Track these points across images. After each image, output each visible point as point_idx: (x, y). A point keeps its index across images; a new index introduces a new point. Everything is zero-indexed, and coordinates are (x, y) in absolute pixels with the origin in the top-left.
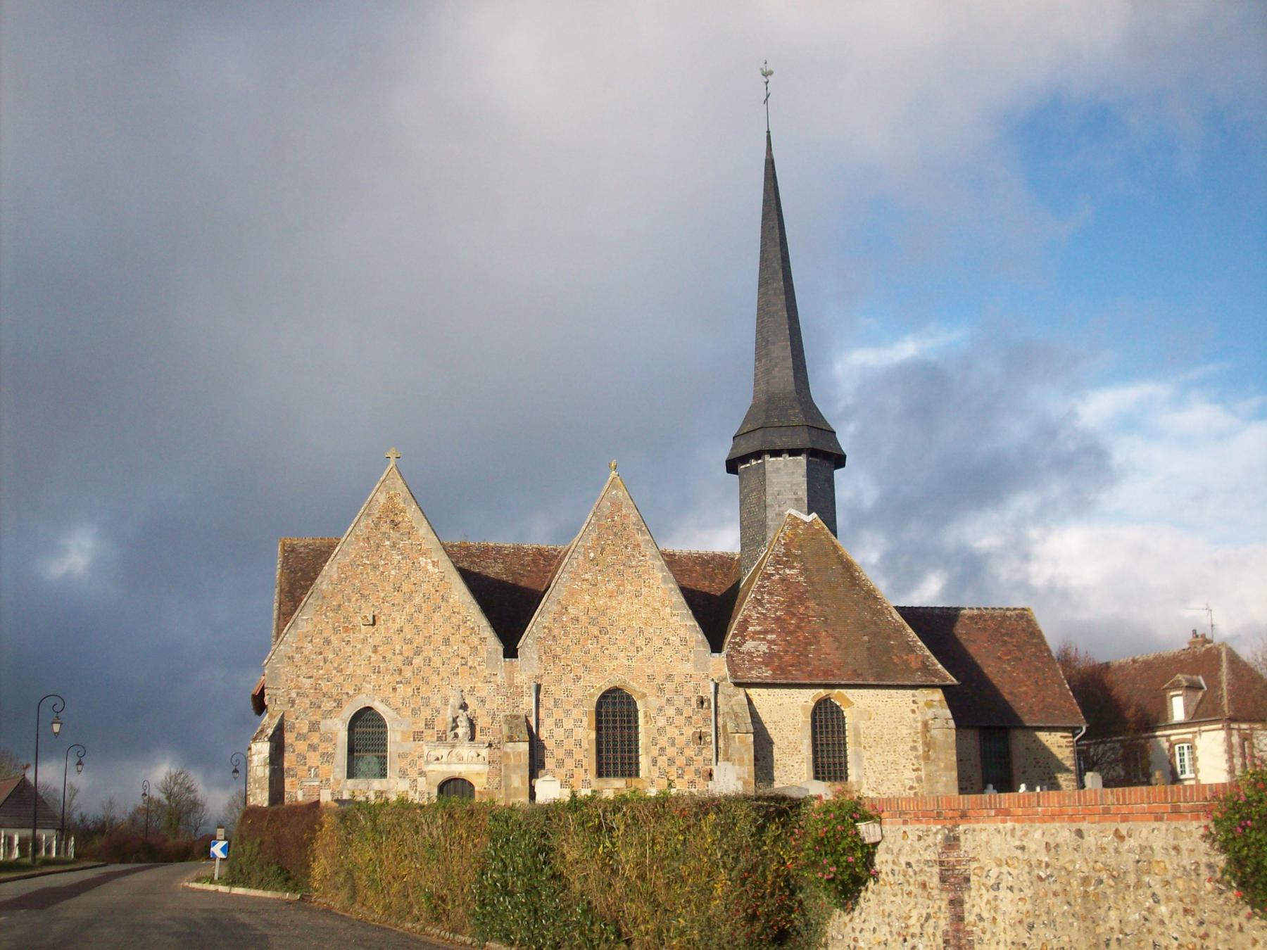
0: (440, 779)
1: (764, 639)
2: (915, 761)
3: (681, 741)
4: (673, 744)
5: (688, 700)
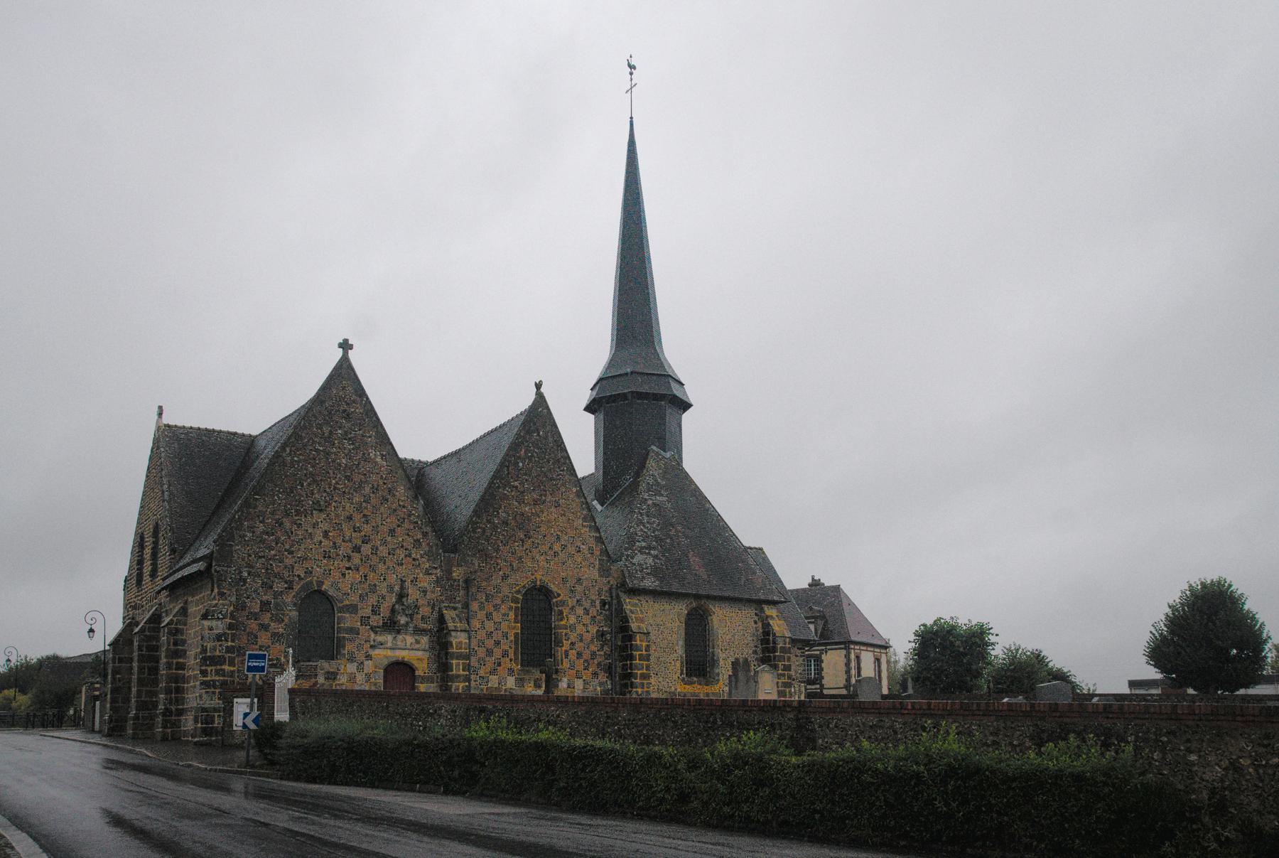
3: (588, 637)
5: (593, 602)
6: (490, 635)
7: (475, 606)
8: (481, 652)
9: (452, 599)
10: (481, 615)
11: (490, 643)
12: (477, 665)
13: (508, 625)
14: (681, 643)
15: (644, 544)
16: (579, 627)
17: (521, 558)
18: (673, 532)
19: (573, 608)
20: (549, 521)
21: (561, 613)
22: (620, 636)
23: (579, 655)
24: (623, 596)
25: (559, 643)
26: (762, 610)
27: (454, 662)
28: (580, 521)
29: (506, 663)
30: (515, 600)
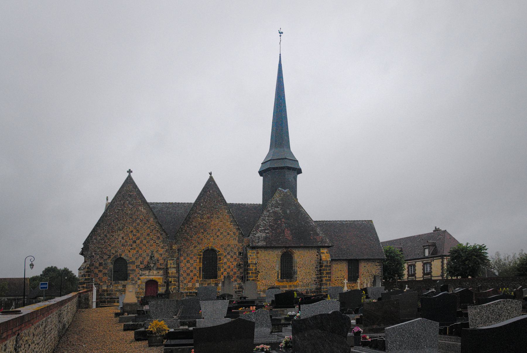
0: (146, 280)
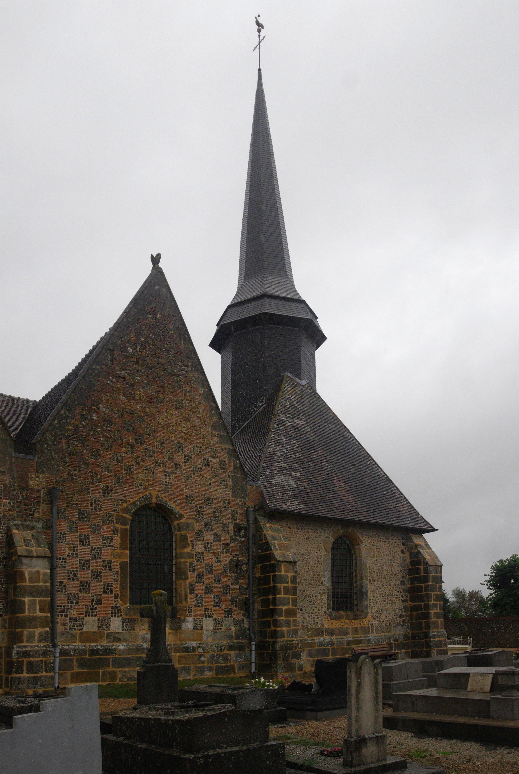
1: (290, 475)
2: (403, 594)
3: (218, 567)
4: (211, 572)
5: (225, 526)
6: (85, 564)
7: (64, 526)
8: (73, 587)
9: (29, 515)
10: (73, 538)
11: (85, 575)
12: (65, 603)
13: (115, 554)
14: (328, 574)
15: (284, 465)
16: (206, 553)
17: (129, 468)
18: (314, 455)
19: (199, 533)
20: (168, 425)
21: (184, 538)
22: (259, 566)
23: (208, 589)
24: (262, 521)
25: (182, 575)
26: (410, 540)
27: (26, 599)
28: (209, 429)
29: (109, 600)
30: (122, 521)
